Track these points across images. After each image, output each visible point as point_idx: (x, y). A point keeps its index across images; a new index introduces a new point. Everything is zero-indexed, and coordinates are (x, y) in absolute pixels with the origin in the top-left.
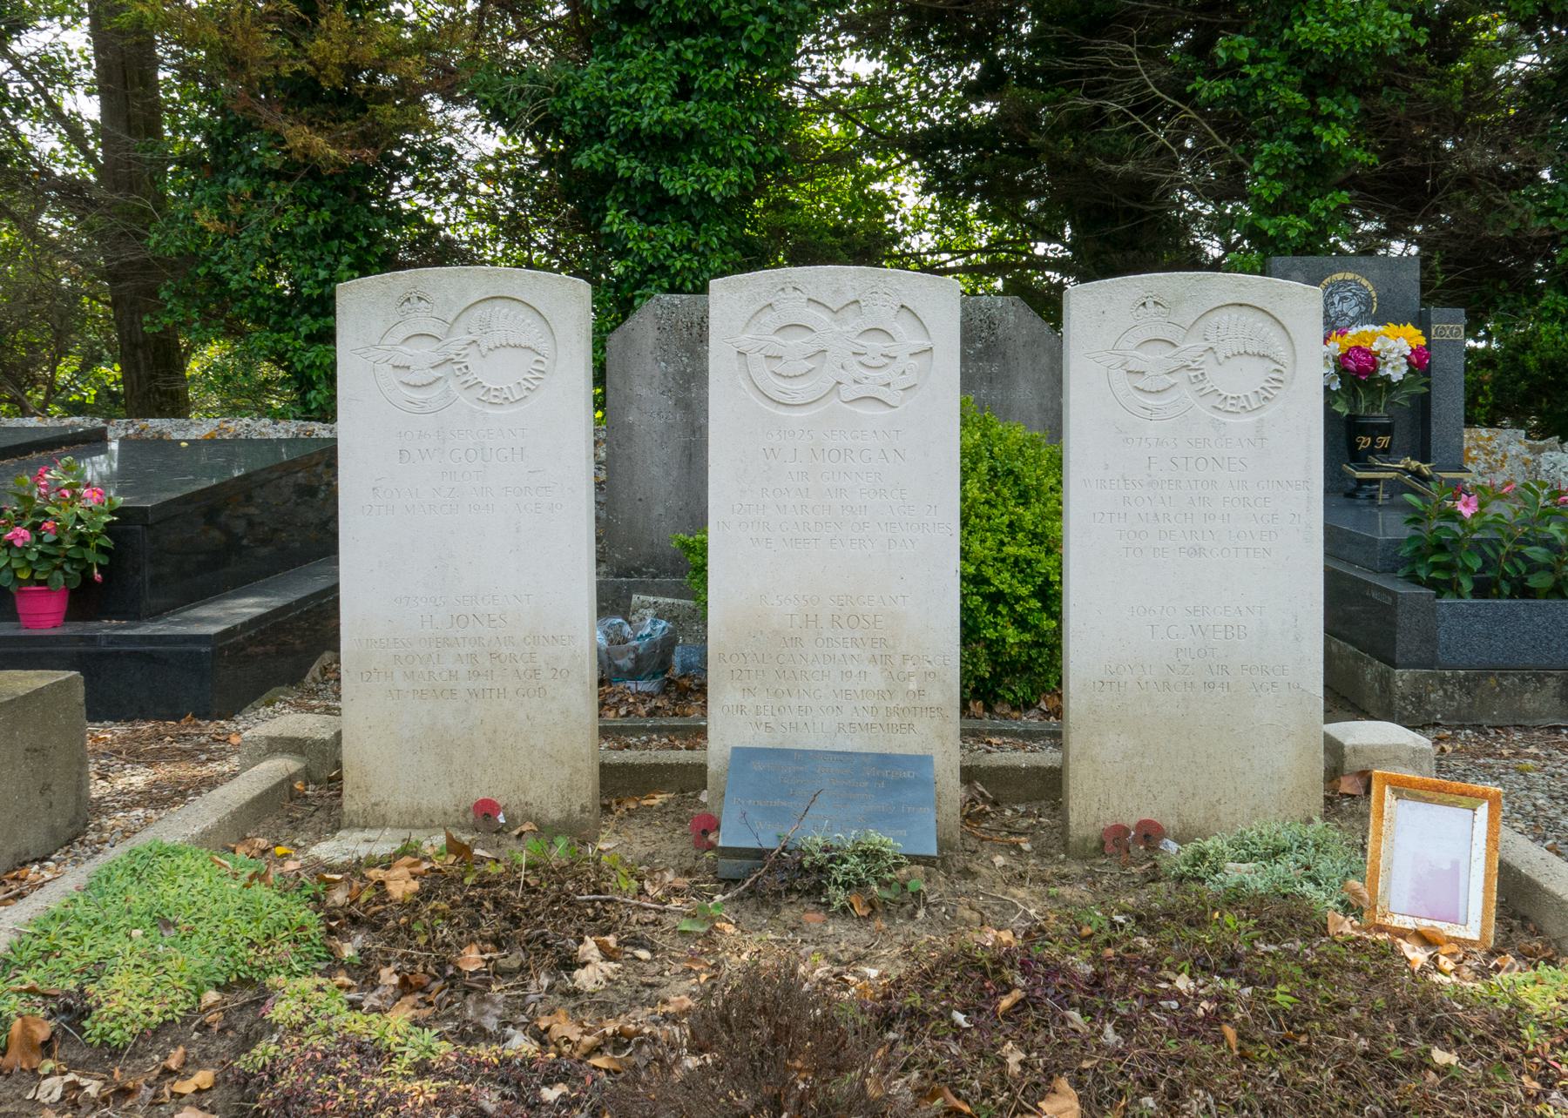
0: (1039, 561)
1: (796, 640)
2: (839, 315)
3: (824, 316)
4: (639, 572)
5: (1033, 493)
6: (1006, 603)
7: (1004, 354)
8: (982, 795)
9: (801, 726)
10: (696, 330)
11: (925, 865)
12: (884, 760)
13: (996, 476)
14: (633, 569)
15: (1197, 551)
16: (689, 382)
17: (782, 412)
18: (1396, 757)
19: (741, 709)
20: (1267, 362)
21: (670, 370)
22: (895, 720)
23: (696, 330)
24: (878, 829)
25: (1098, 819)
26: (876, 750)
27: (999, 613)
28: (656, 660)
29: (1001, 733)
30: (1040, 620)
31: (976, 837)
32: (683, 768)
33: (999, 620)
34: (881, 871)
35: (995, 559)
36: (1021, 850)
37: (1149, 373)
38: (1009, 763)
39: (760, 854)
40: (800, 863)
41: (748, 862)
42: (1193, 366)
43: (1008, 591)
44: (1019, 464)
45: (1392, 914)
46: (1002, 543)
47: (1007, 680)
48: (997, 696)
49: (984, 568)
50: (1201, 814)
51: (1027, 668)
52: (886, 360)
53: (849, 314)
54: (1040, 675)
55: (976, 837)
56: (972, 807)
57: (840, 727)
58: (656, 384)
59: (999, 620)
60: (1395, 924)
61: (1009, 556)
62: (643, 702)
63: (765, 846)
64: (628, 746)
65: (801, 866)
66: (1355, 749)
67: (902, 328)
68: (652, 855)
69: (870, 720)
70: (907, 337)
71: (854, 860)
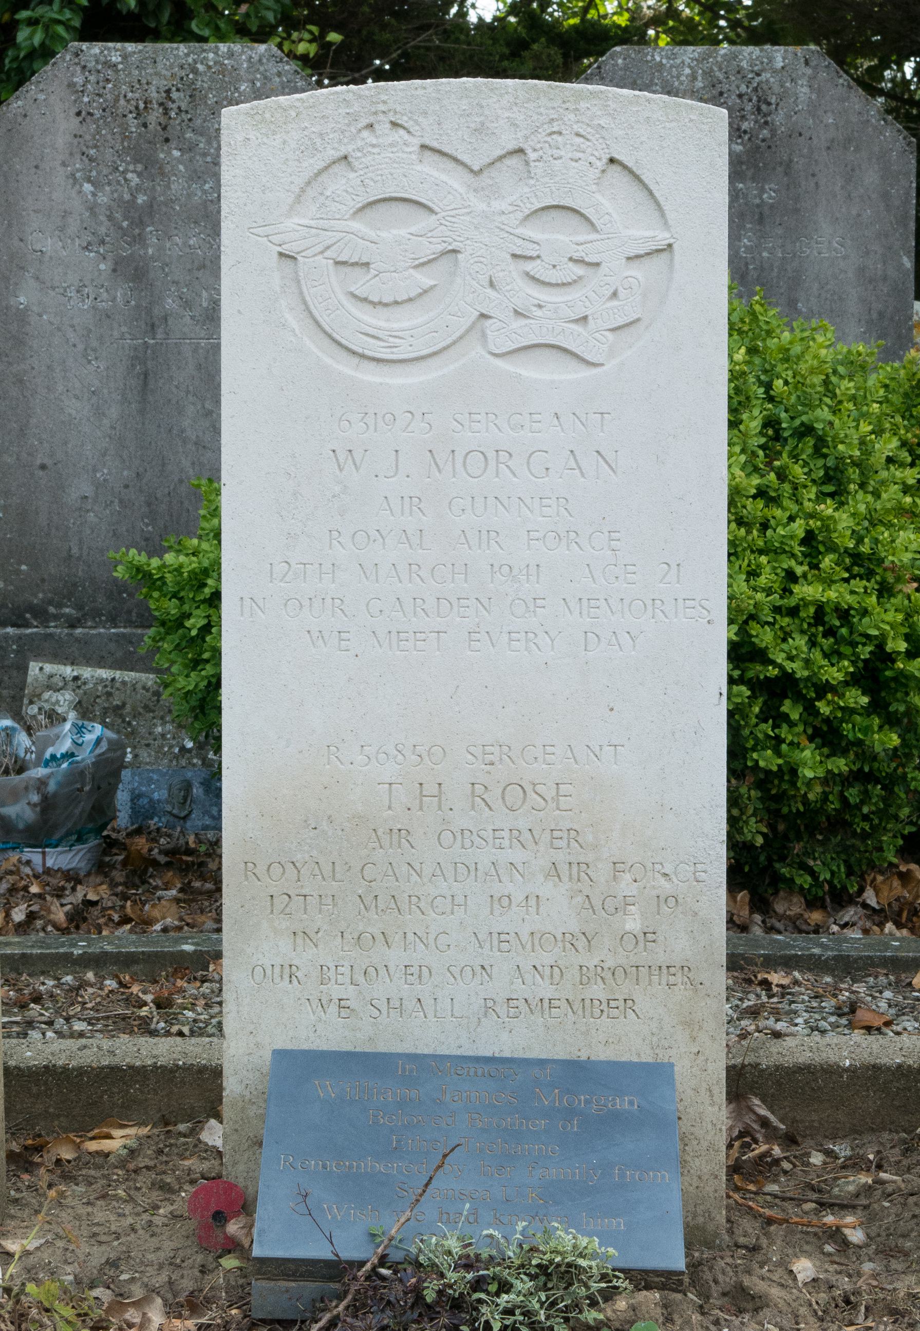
0: (865, 612)
1: (401, 834)
2: (485, 179)
3: (454, 180)
4: (41, 615)
5: (853, 473)
6: (799, 697)
7: (789, 165)
8: (764, 1123)
9: (410, 1004)
10: (154, 117)
11: (662, 1287)
12: (577, 1072)
13: (777, 437)
14: (31, 609)
16: (141, 224)
17: (370, 375)
19: (290, 972)
21: (103, 199)
22: (597, 991)
23: (154, 117)
24: (569, 1222)
26: (560, 1054)
27: (786, 717)
28: (81, 808)
29: (789, 963)
30: (866, 730)
31: (756, 1216)
32: (167, 1075)
33: (784, 732)
34: (577, 1306)
35: (777, 610)
36: (845, 1244)
38: (817, 1059)
39: (335, 1270)
40: (417, 1292)
41: (311, 1288)
43: (802, 673)
44: (824, 413)
46: (791, 577)
47: (797, 848)
48: (777, 880)
49: (754, 629)
51: (838, 823)
52: (580, 270)
53: (504, 175)
54: (865, 836)
55: (756, 1216)
56: (746, 1147)
57: (489, 1006)
58: (74, 225)
59: (784, 732)
61: (805, 603)
62: (59, 893)
63: (345, 1255)
64: (37, 999)
65: (419, 1298)
67: (610, 203)
68: (113, 1264)
69: (546, 990)
70: (623, 222)
71: (523, 1284)
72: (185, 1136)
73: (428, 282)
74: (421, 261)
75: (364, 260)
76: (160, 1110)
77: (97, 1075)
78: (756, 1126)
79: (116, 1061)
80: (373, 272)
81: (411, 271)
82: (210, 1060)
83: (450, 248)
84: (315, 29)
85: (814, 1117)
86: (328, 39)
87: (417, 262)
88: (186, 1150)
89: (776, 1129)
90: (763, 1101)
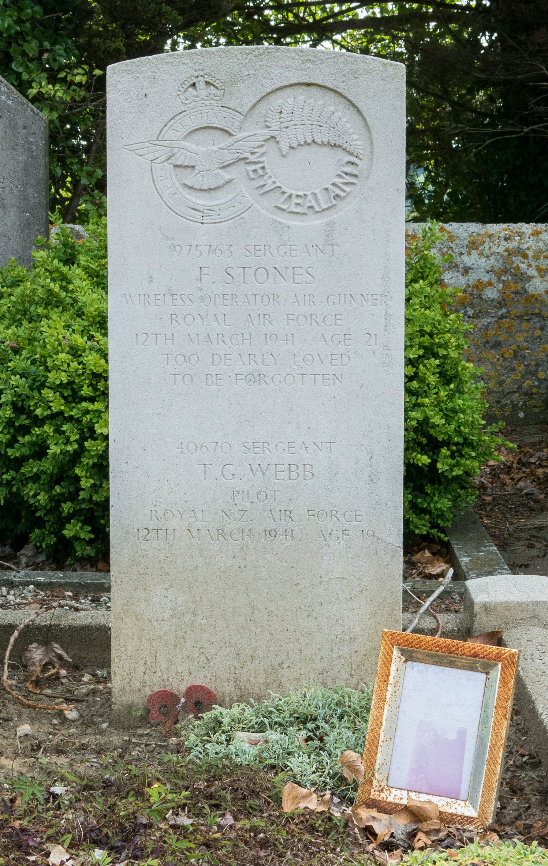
8: (60, 658)
15: (258, 378)
18: (535, 617)
20: (340, 155)
25: (143, 684)
37: (199, 168)
42: (252, 158)
45: (390, 788)
50: (261, 679)
60: (390, 799)
66: (486, 608)
73: (228, 177)
74: (225, 164)
78: (55, 660)
81: (219, 170)
83: (242, 156)
84: (86, 67)
85: (92, 655)
86: (94, 73)
87: (222, 165)
89: (66, 661)
90: (62, 646)
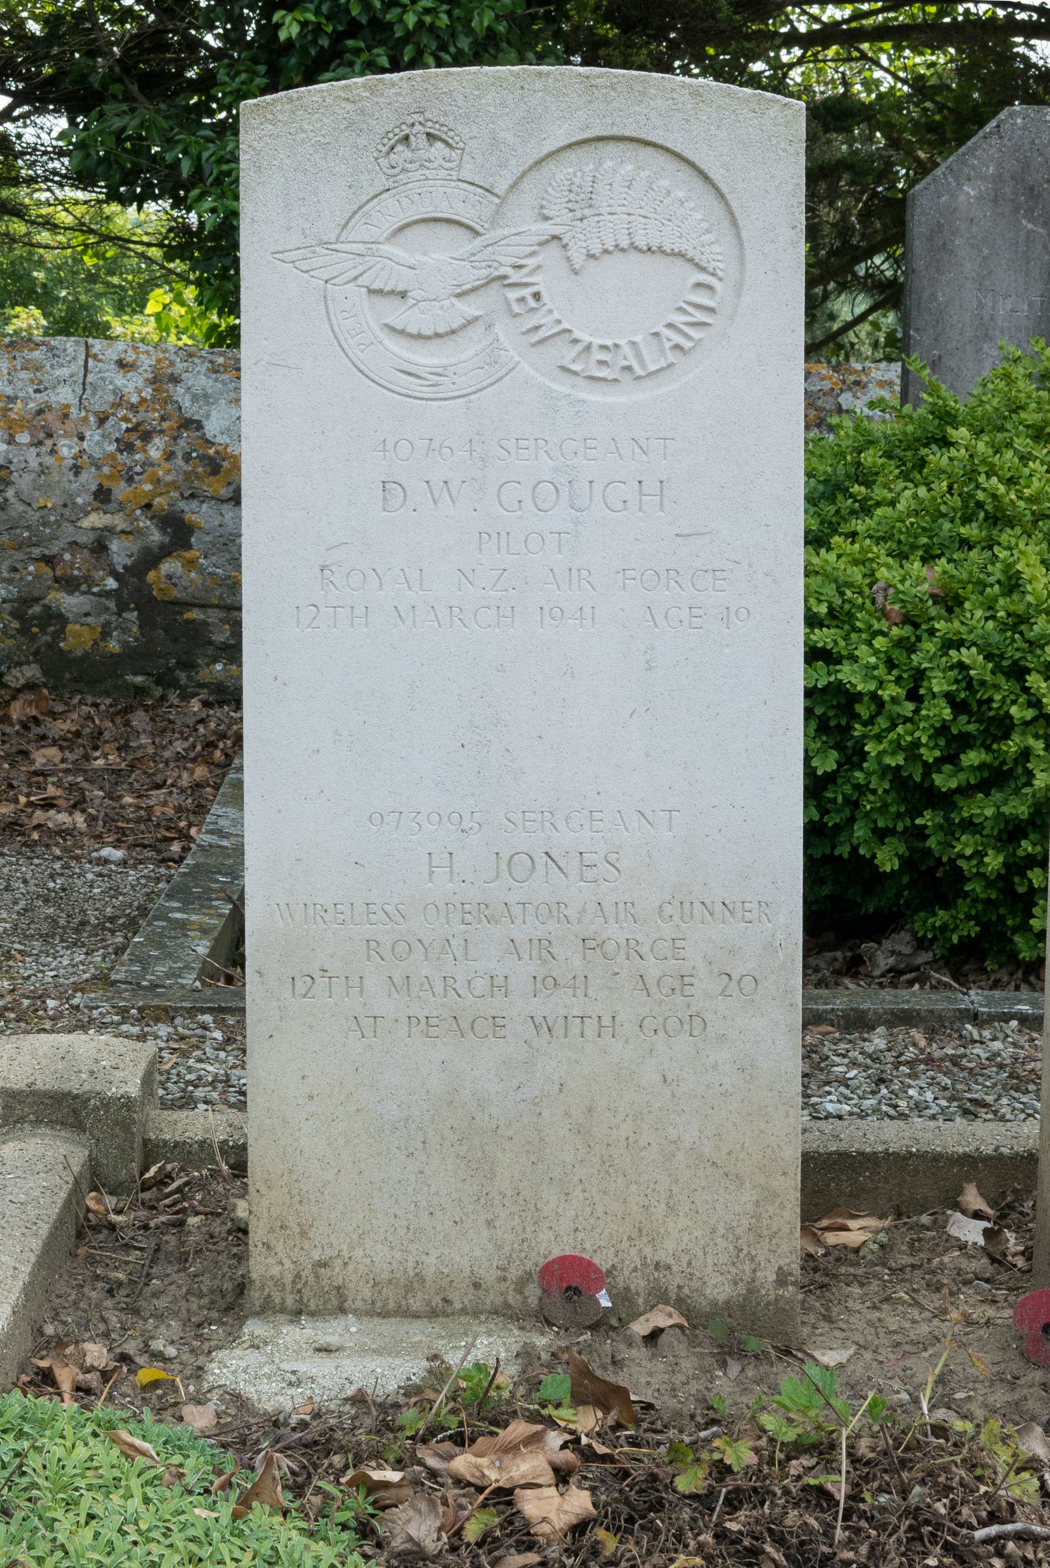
72: (928, 1229)
74: (464, 288)
75: (400, 288)
76: (891, 1200)
77: (824, 1162)
79: (843, 1146)
80: (411, 302)
82: (944, 1147)
83: (496, 273)
88: (937, 1245)
